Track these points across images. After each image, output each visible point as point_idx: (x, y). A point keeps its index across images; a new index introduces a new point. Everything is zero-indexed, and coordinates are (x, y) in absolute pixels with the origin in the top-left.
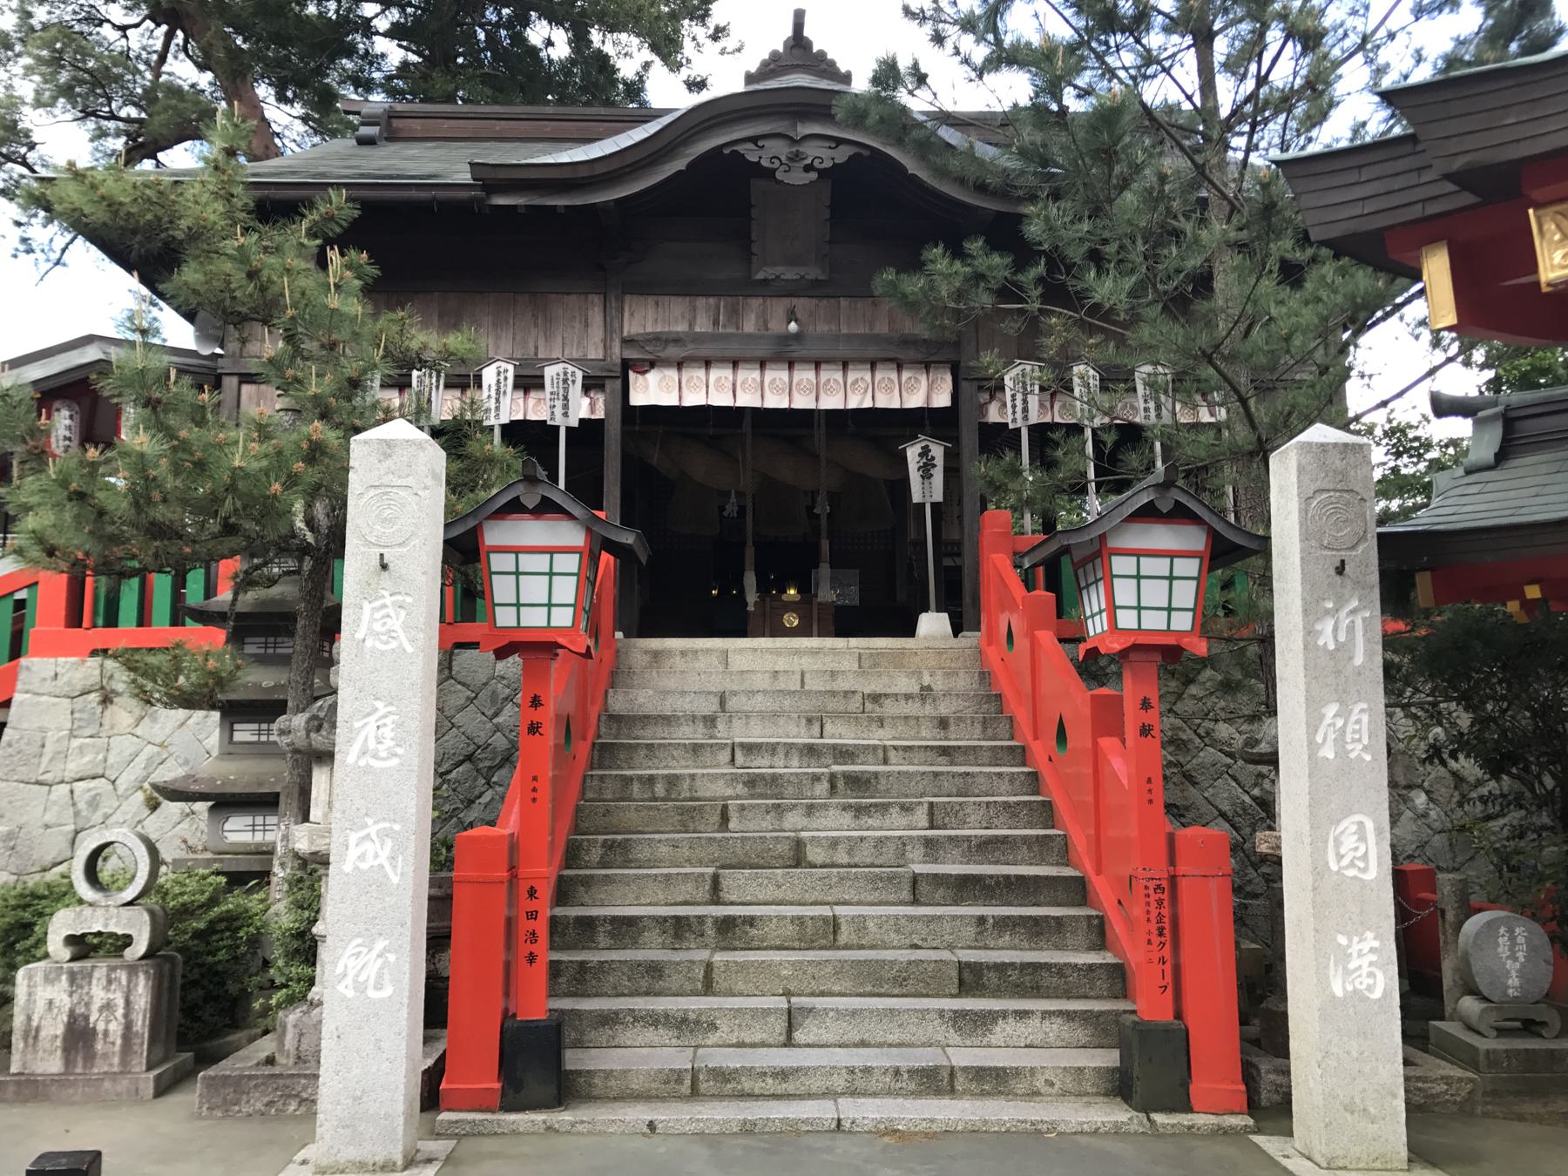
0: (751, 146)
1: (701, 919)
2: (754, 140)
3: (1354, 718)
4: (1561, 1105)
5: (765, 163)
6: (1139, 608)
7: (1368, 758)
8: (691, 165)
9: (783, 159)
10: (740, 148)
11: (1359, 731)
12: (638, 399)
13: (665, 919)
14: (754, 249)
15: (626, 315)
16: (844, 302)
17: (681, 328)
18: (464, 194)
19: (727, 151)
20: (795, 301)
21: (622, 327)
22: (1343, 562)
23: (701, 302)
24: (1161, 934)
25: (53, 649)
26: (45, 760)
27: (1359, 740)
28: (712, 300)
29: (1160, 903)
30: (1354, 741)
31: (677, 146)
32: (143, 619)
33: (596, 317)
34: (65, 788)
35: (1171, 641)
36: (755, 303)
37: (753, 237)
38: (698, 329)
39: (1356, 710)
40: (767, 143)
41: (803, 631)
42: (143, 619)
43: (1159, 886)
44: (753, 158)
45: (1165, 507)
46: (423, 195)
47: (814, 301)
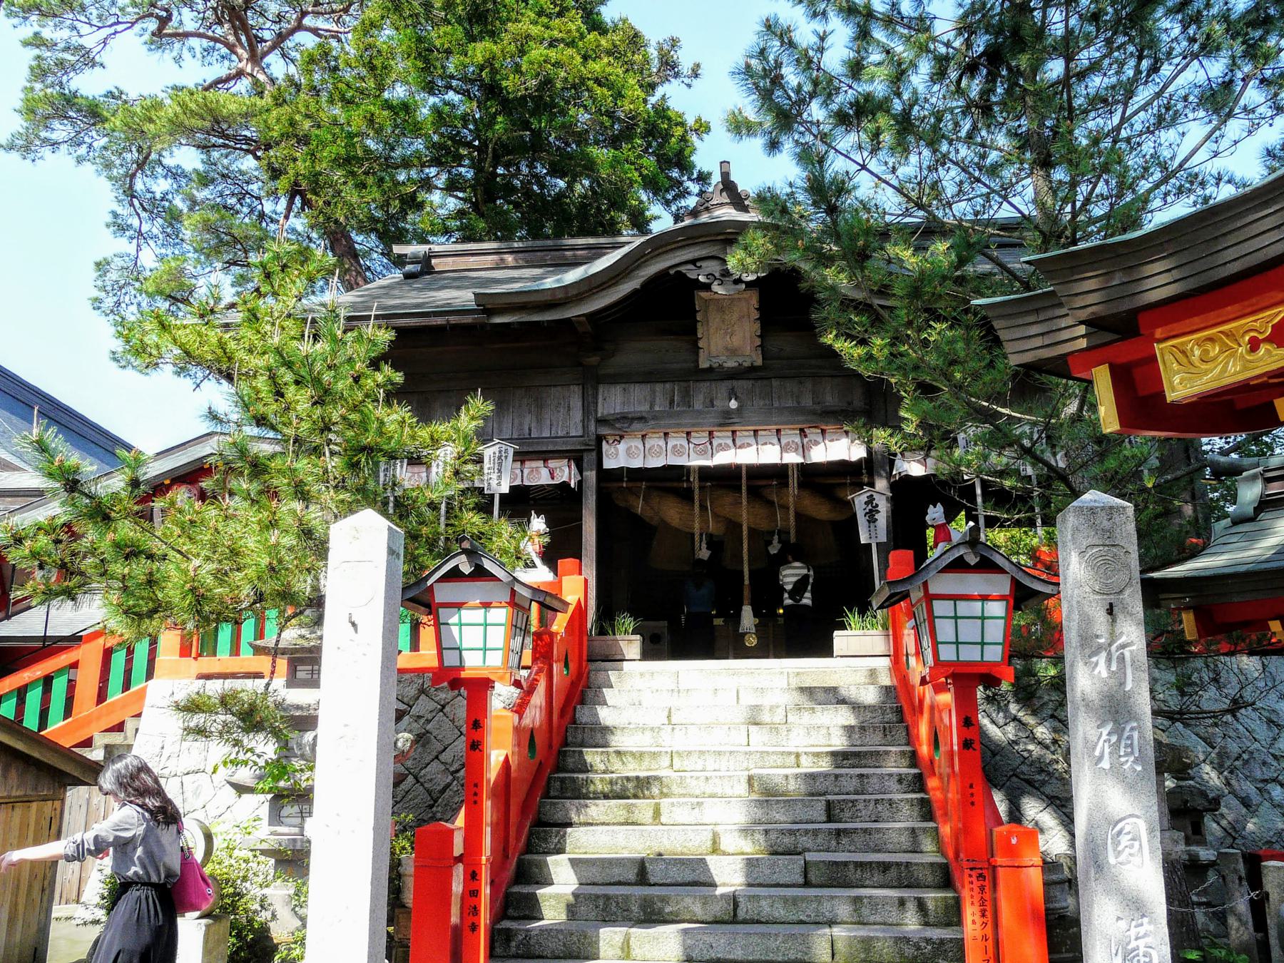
0: (691, 267)
1: (627, 898)
2: (693, 262)
3: (1126, 734)
4: (136, 961)
5: (702, 278)
6: (957, 643)
7: (1139, 768)
8: (647, 284)
9: (717, 275)
10: (682, 269)
11: (1131, 745)
12: (609, 464)
13: (598, 897)
14: (700, 345)
15: (600, 400)
16: (775, 383)
17: (645, 408)
18: (468, 319)
19: (672, 272)
20: (735, 383)
21: (596, 411)
22: (1111, 605)
23: (659, 387)
24: (983, 915)
25: (174, 672)
26: (164, 758)
27: (1132, 753)
28: (668, 386)
29: (982, 889)
30: (1126, 755)
31: (632, 271)
32: (235, 651)
33: (576, 403)
34: (177, 780)
35: (984, 670)
36: (704, 386)
37: (699, 335)
38: (657, 408)
39: (1128, 729)
40: (704, 264)
41: (762, 652)
42: (235, 651)
43: (980, 875)
44: (692, 276)
45: (972, 560)
46: (440, 321)
47: (750, 383)
